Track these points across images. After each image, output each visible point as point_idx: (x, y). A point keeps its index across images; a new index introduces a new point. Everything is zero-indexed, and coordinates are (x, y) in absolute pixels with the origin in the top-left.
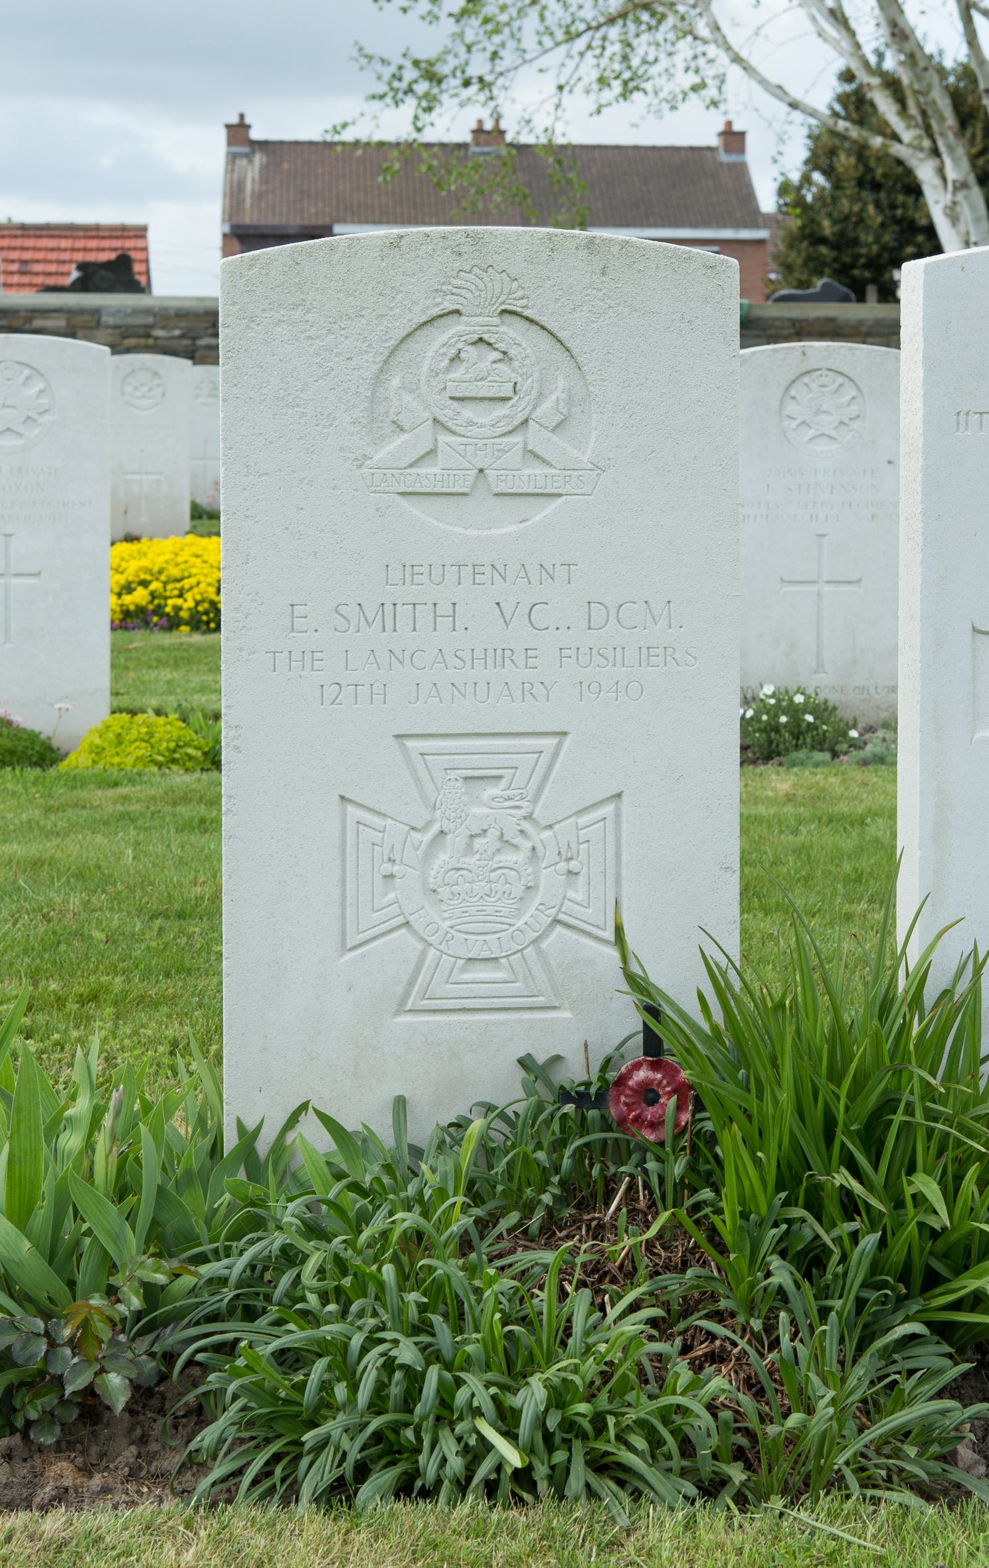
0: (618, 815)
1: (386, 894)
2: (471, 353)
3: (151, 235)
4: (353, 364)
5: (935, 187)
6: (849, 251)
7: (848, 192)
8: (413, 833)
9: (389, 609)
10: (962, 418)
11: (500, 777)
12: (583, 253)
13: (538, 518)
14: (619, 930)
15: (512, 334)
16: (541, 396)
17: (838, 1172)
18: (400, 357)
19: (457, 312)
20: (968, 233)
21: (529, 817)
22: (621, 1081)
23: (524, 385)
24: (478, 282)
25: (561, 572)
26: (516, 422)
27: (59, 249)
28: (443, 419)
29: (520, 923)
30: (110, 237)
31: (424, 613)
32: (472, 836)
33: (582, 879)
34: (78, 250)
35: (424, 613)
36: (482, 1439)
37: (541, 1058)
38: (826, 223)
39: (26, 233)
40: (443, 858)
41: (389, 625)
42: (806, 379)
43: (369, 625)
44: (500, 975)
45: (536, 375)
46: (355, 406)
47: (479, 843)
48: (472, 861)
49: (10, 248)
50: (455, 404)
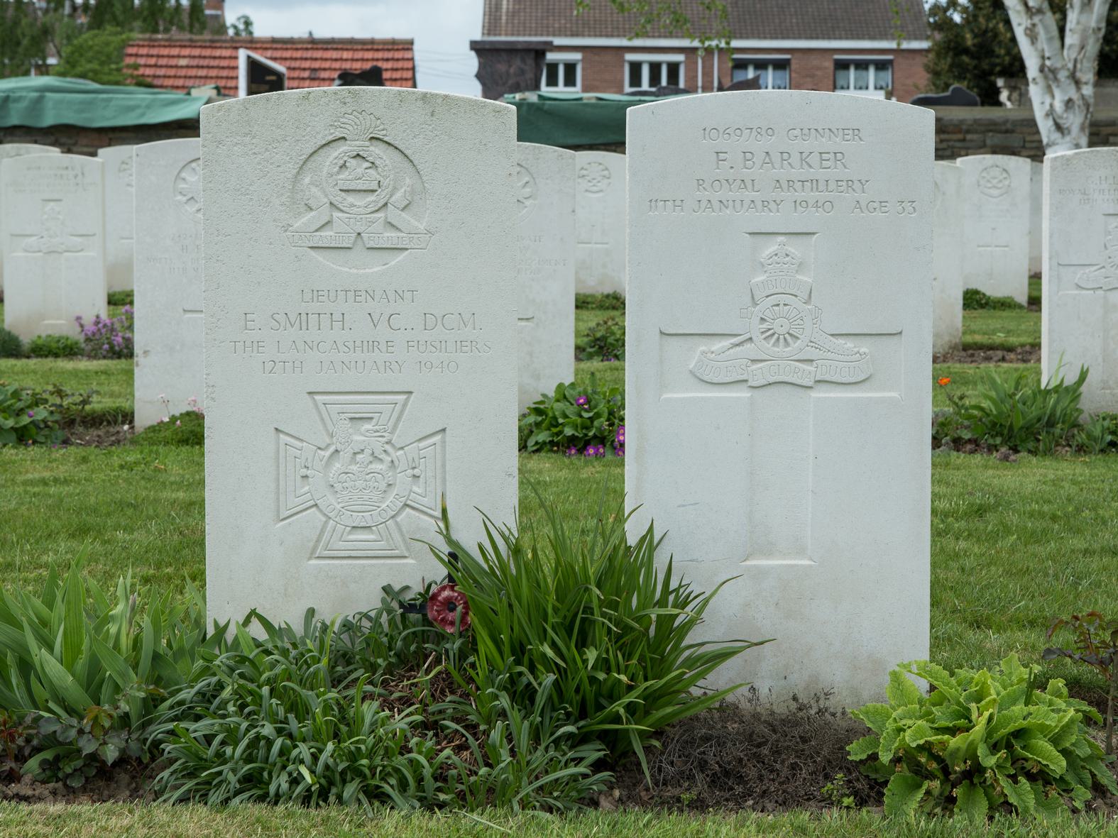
0: (444, 442)
1: (303, 487)
2: (354, 162)
3: (416, 47)
4: (280, 169)
5: (1018, 12)
6: (987, 61)
7: (985, 12)
8: (319, 451)
9: (304, 316)
10: (653, 203)
11: (372, 418)
12: (420, 103)
13: (393, 263)
14: (444, 511)
15: (377, 151)
16: (395, 189)
17: (849, 753)
18: (309, 164)
19: (344, 138)
20: (1043, 50)
21: (388, 443)
22: (434, 597)
23: (385, 183)
24: (356, 120)
25: (408, 295)
26: (380, 205)
27: (341, 59)
28: (336, 203)
29: (384, 506)
30: (383, 50)
31: (325, 320)
32: (355, 454)
33: (421, 480)
34: (357, 60)
35: (325, 320)
36: (300, 774)
37: (397, 587)
38: (968, 36)
39: (315, 46)
40: (337, 465)
41: (304, 327)
42: (194, 165)
43: (292, 326)
44: (372, 537)
45: (392, 176)
46: (282, 195)
47: (359, 457)
48: (354, 468)
49: (292, 59)
50: (343, 194)
